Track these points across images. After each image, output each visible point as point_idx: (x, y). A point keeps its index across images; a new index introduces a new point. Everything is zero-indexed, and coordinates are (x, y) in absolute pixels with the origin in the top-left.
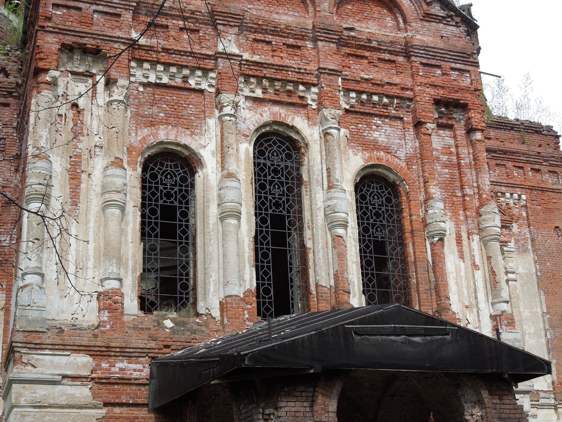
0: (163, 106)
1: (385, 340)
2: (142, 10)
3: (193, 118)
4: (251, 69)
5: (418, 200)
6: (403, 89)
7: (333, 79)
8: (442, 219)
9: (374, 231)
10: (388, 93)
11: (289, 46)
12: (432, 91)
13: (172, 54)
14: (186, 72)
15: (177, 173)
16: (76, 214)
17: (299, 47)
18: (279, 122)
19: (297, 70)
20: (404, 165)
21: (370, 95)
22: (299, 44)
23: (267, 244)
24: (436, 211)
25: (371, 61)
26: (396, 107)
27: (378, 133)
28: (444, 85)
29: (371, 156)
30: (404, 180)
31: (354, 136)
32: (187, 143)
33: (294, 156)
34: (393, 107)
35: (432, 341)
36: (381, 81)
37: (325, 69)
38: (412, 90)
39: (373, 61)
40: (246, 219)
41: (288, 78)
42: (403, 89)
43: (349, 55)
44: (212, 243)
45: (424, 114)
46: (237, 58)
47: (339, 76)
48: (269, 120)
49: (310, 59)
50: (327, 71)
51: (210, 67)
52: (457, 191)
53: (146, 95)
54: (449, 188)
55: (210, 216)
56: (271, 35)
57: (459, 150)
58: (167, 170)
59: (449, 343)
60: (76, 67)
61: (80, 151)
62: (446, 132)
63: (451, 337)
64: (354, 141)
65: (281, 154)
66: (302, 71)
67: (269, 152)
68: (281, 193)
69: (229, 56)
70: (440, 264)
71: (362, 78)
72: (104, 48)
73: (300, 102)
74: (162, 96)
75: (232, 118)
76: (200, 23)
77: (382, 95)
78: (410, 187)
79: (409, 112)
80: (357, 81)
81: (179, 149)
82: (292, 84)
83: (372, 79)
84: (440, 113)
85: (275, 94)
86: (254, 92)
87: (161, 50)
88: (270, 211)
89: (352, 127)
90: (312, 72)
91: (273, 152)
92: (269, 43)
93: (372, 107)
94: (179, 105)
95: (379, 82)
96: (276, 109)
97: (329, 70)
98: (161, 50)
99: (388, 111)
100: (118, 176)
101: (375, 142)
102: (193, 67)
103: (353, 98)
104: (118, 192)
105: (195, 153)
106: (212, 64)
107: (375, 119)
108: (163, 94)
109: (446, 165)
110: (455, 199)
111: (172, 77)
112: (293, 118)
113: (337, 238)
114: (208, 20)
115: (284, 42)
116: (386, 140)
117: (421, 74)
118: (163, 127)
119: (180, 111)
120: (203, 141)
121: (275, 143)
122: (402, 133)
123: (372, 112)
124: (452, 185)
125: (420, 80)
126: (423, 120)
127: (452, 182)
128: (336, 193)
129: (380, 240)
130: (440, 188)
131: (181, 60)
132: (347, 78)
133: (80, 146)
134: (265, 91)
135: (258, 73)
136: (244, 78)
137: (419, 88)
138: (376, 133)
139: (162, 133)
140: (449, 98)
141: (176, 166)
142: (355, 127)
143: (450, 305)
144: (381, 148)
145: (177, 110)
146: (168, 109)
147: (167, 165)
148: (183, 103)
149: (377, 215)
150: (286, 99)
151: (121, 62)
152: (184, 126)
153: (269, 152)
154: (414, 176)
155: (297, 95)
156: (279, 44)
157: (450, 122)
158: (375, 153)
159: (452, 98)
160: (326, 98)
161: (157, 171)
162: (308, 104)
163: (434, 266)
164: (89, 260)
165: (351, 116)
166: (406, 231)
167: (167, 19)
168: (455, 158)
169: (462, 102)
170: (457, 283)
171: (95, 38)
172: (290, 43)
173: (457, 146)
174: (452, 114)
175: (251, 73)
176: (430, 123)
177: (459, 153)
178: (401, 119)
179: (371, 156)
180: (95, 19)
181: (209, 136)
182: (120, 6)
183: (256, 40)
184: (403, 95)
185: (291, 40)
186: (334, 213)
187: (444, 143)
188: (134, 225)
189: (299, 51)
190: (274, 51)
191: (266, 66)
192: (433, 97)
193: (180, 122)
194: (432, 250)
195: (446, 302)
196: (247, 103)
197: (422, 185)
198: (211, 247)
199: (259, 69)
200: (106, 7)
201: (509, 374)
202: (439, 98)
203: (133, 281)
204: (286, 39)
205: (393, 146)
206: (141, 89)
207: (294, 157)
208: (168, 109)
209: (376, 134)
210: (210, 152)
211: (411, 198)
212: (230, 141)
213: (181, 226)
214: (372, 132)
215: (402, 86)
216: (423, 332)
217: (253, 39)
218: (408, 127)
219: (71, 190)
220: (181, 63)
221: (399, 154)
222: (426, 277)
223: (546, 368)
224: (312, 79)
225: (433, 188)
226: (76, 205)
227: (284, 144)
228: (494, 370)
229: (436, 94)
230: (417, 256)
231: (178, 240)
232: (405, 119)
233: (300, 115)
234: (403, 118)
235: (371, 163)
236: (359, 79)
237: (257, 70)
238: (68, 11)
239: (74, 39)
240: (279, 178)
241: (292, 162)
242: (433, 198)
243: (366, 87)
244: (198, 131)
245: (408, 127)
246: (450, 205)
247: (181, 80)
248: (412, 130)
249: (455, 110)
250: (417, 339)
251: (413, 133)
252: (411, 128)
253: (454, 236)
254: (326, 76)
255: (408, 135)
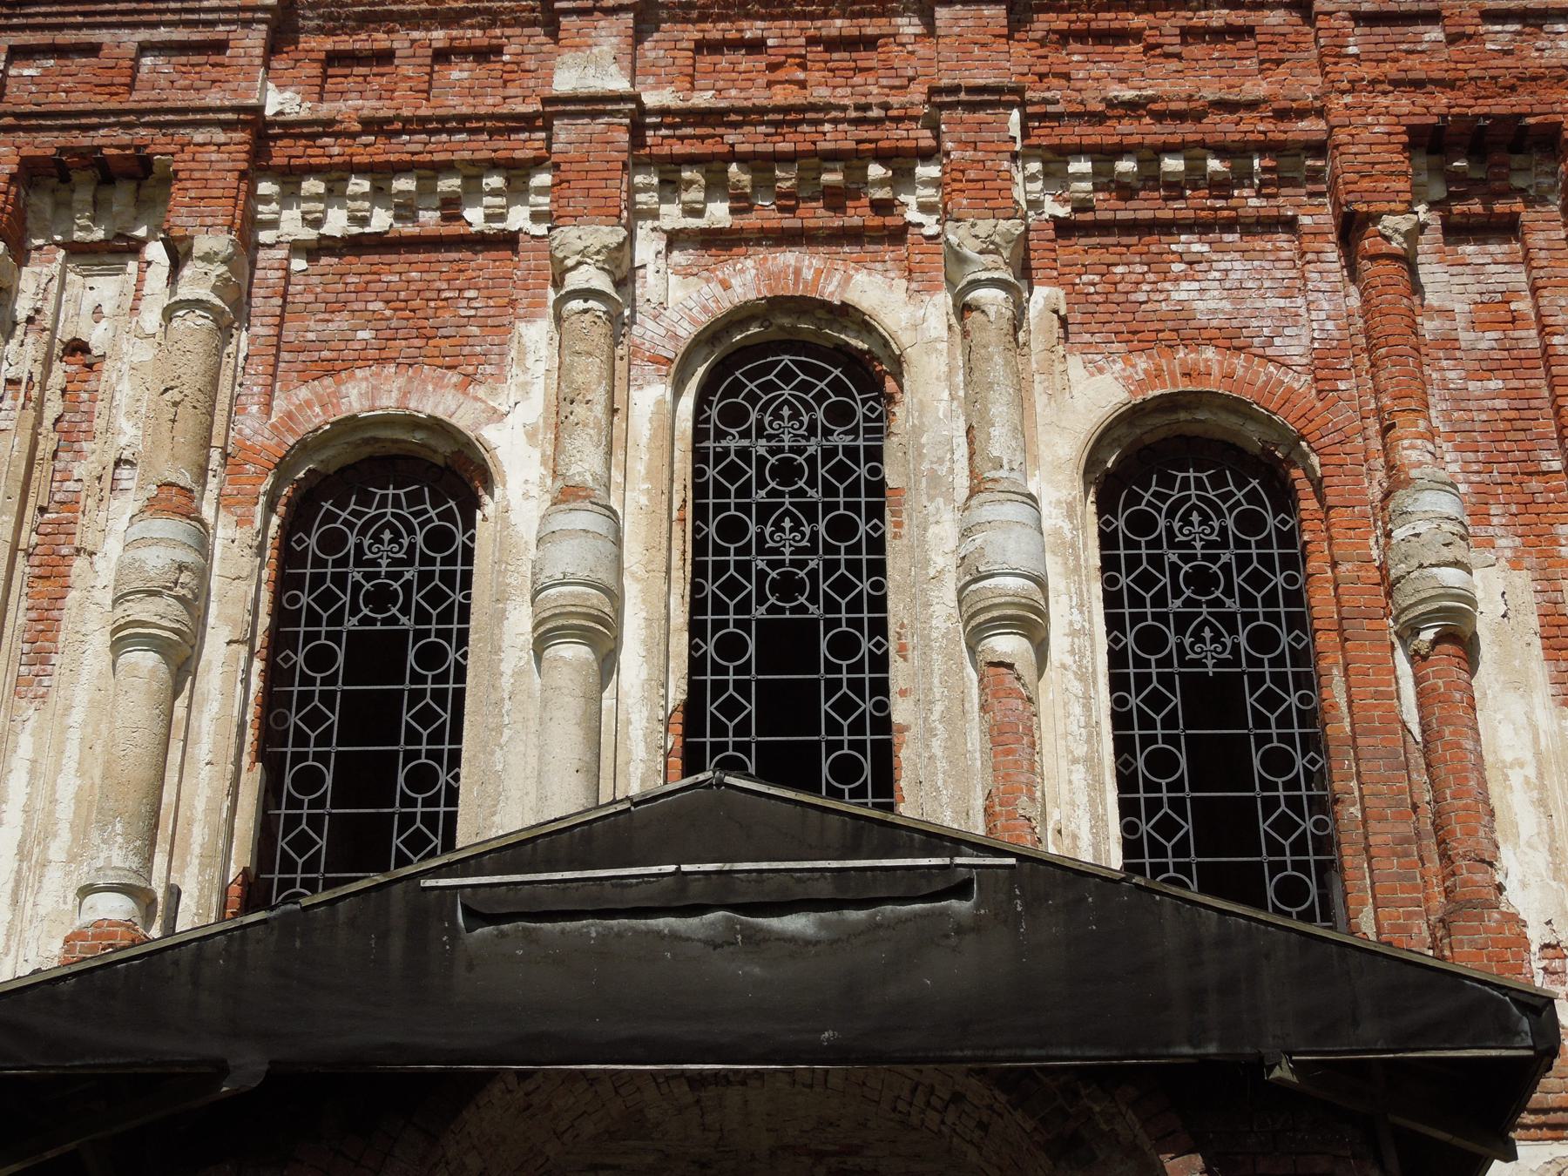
0: (371, 306)
1: (619, 935)
2: (305, 18)
3: (475, 330)
4: (682, 138)
5: (1363, 503)
6: (1282, 115)
7: (991, 118)
8: (1448, 554)
9: (1187, 641)
10: (1219, 137)
11: (833, 44)
12: (1407, 104)
13: (398, 133)
14: (449, 184)
15: (415, 522)
16: (42, 691)
17: (870, 43)
18: (792, 297)
19: (853, 114)
20: (1300, 383)
21: (1151, 154)
22: (869, 31)
23: (742, 729)
24: (1422, 528)
25: (1152, 40)
26: (1263, 184)
27: (1195, 285)
28: (1452, 75)
29: (1159, 369)
30: (1303, 437)
31: (1092, 308)
32: (440, 413)
33: (860, 411)
34: (1251, 186)
35: (874, 926)
36: (1190, 98)
37: (955, 90)
38: (1321, 113)
39: (1161, 40)
40: (644, 642)
41: (822, 145)
42: (1282, 115)
43: (1065, 37)
44: (503, 740)
45: (1365, 184)
46: (621, 106)
47: (1010, 105)
48: (752, 296)
49: (911, 73)
50: (963, 96)
51: (530, 154)
52: (1547, 455)
53: (315, 280)
54: (1505, 446)
55: (505, 645)
56: (762, 18)
57: (1543, 302)
58: (384, 514)
59: (960, 930)
60: (82, 228)
61: (78, 486)
62: (1492, 248)
63: (978, 906)
64: (1094, 328)
65: (809, 408)
66: (875, 113)
67: (763, 409)
68: (1226, 655)
69: (591, 105)
70: (1447, 731)
71: (1111, 103)
72: (159, 149)
73: (877, 221)
74: (369, 277)
75: (592, 304)
76: (504, 25)
77: (1198, 152)
78: (1326, 460)
79: (1322, 194)
80: (1093, 114)
81: (418, 437)
82: (838, 166)
83: (1152, 99)
84: (1452, 178)
85: (781, 209)
86: (699, 213)
87: (357, 127)
88: (759, 612)
89: (1085, 278)
90: (910, 112)
91: (780, 407)
92: (756, 46)
93: (1166, 199)
94: (428, 295)
95: (1183, 106)
96: (788, 258)
97: (972, 90)
98: (357, 127)
99: (1233, 203)
100: (157, 542)
101: (1183, 314)
102: (473, 163)
103: (1081, 177)
104: (151, 593)
105: (469, 443)
106: (537, 144)
107: (1183, 238)
108: (374, 268)
109: (1494, 365)
110: (1534, 484)
111: (405, 211)
112: (847, 279)
113: (993, 670)
114: (533, 10)
115: (812, 32)
116: (1227, 305)
117: (1352, 50)
118: (367, 372)
119: (430, 312)
120: (502, 398)
121: (787, 376)
122: (1293, 273)
123: (1167, 214)
124: (1521, 436)
125: (1348, 71)
126: (1363, 208)
127: (1519, 424)
128: (986, 507)
129: (1211, 671)
130: (1459, 449)
131: (431, 147)
132: (1051, 109)
133: (79, 470)
134: (741, 204)
135: (709, 147)
136: (661, 172)
137: (1348, 99)
138: (1184, 285)
139: (354, 393)
140: (1477, 116)
141: (414, 498)
142: (1097, 279)
143: (1500, 888)
144: (1206, 334)
145: (420, 314)
146: (388, 313)
147: (384, 497)
148: (445, 286)
149: (1202, 580)
150: (817, 216)
151: (211, 184)
152: (439, 361)
153: (763, 409)
154: (1343, 415)
155: (865, 201)
156: (791, 42)
157: (1499, 207)
158: (1181, 355)
159: (1486, 116)
160: (957, 186)
161: (346, 522)
162: (910, 223)
163: (1426, 743)
164: (55, 836)
165: (1083, 241)
166: (1317, 624)
167: (388, 32)
168: (1533, 333)
169: (1531, 121)
170: (1542, 803)
171: (128, 126)
172: (835, 32)
173: (1534, 290)
174: (1505, 178)
175: (678, 148)
176: (1392, 213)
177: (1544, 311)
178: (1290, 225)
179: (1159, 369)
180: (144, 70)
181: (522, 378)
182: (223, 16)
183: (701, 47)
184: (1283, 137)
185: (838, 22)
186: (976, 581)
187: (1484, 288)
188: (223, 706)
189: (873, 54)
190: (773, 67)
191: (733, 117)
192: (1404, 120)
193: (428, 351)
194: (1418, 681)
195: (1478, 877)
196: (676, 253)
197: (1376, 444)
198: (498, 753)
199: (711, 131)
200: (180, 29)
201: (1298, 1068)
202: (1433, 120)
203: (200, 897)
204: (819, 23)
205: (1254, 323)
206: (299, 264)
207: (859, 415)
208: (388, 313)
209: (1184, 292)
210: (520, 430)
211: (1330, 500)
212: (580, 379)
213: (417, 696)
214: (1167, 286)
215: (1275, 105)
216: (825, 890)
217: (697, 42)
218: (1317, 246)
219: (33, 615)
220: (428, 157)
221: (1280, 347)
222: (1401, 791)
223: (1525, 1024)
224: (912, 134)
225: (1412, 447)
226: (45, 662)
227: (821, 374)
228: (1212, 1049)
229: (1418, 110)
230: (1360, 714)
231: (402, 747)
232: (1305, 220)
233: (879, 266)
234: (1295, 218)
235: (1157, 392)
236: (1101, 107)
237: (702, 138)
238: (62, 62)
239: (63, 139)
240: (1218, 603)
241: (854, 432)
242: (1409, 482)
243: (1132, 129)
244: (489, 369)
245: (1317, 246)
246: (1514, 509)
247: (438, 214)
248: (1334, 256)
249: (1517, 160)
250: (797, 923)
251: (1337, 265)
252: (1329, 247)
253: (1534, 622)
254: (959, 113)
255: (1315, 276)
